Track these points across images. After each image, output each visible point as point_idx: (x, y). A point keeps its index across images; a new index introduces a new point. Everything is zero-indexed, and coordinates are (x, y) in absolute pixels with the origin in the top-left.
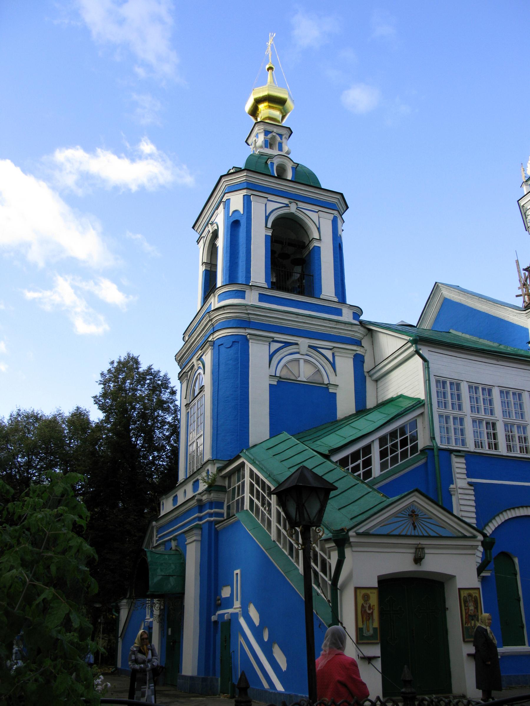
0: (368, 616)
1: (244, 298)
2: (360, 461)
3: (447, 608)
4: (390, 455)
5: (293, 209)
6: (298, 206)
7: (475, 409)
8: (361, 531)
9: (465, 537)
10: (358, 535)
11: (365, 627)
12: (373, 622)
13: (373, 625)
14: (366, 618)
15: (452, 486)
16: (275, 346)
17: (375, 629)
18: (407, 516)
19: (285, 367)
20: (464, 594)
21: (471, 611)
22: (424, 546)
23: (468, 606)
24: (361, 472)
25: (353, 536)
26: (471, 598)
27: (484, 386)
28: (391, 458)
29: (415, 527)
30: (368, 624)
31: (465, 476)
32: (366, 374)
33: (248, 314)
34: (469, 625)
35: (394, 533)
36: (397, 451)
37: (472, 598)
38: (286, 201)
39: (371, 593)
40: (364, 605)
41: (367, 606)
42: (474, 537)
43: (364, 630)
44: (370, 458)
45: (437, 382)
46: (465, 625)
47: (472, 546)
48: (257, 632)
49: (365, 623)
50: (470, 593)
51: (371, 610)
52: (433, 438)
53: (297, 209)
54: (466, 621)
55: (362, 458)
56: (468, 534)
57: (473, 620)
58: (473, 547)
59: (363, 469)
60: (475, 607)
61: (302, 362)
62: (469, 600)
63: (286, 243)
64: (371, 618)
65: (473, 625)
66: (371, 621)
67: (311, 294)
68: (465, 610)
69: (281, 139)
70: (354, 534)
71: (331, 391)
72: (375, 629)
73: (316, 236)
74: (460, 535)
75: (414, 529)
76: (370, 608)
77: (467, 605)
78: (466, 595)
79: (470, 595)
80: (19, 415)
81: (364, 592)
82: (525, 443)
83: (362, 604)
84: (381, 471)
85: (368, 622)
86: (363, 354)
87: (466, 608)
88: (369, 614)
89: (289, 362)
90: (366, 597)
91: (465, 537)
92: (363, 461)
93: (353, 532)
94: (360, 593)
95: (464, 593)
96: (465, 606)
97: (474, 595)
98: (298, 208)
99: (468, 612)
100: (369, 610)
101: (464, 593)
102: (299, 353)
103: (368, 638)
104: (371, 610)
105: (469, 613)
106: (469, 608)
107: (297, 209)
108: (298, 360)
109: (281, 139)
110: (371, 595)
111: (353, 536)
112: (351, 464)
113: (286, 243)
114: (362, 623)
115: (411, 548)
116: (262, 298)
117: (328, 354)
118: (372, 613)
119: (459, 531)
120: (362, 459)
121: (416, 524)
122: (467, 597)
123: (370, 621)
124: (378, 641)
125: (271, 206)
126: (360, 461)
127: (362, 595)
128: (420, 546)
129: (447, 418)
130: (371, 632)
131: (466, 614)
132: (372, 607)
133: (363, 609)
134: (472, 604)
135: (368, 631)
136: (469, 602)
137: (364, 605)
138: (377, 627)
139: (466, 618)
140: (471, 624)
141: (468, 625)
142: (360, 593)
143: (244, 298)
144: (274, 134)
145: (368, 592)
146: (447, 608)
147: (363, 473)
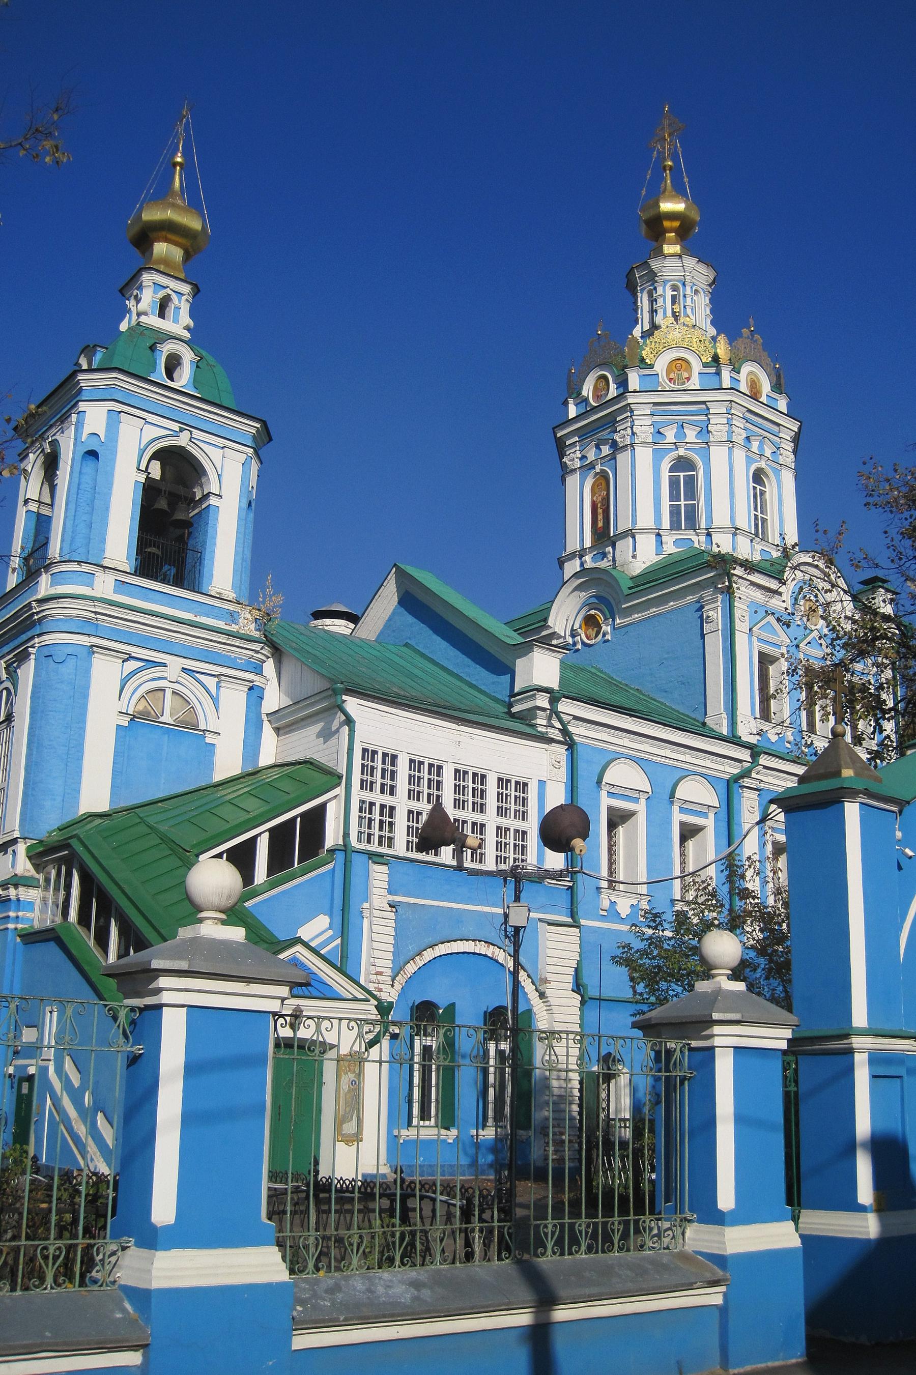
1: (91, 585)
5: (183, 440)
6: (193, 436)
7: (501, 811)
9: (355, 999)
15: (365, 905)
16: (133, 665)
19: (143, 699)
27: (432, 761)
31: (385, 892)
32: (264, 717)
33: (96, 613)
38: (176, 427)
45: (365, 751)
48: (76, 1097)
52: (346, 835)
53: (190, 441)
61: (168, 693)
63: (165, 491)
67: (194, 588)
69: (180, 301)
71: (208, 740)
73: (214, 488)
82: (523, 806)
86: (263, 686)
89: (148, 692)
91: (355, 999)
98: (193, 440)
102: (166, 679)
107: (190, 441)
108: (163, 690)
109: (180, 301)
113: (165, 491)
116: (120, 585)
117: (211, 683)
125: (151, 432)
129: (372, 804)
143: (91, 585)
144: (170, 292)
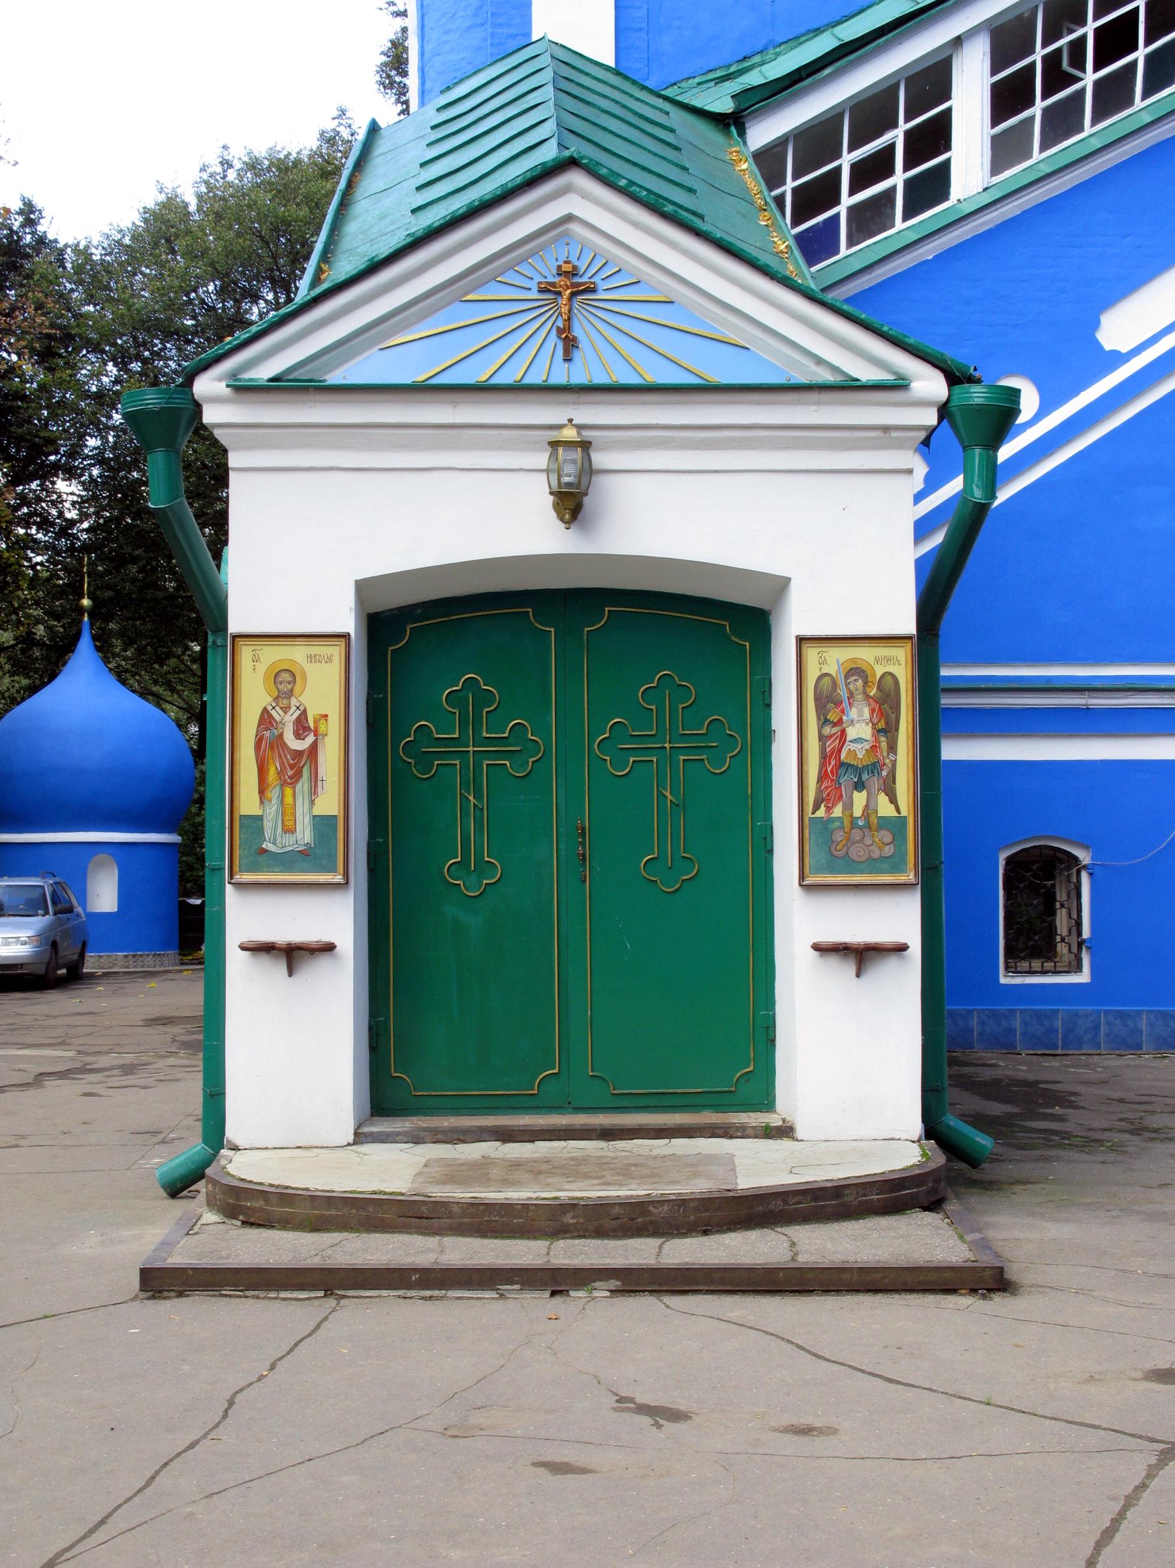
0: (292, 767)
2: (897, 136)
3: (774, 731)
4: (1044, 98)
8: (264, 373)
9: (850, 387)
10: (243, 389)
11: (271, 810)
12: (314, 791)
13: (312, 802)
14: (280, 774)
17: (323, 825)
18: (536, 295)
20: (834, 660)
21: (853, 747)
22: (588, 434)
23: (840, 721)
24: (899, 179)
25: (217, 400)
26: (860, 683)
28: (1046, 112)
29: (570, 344)
30: (289, 799)
34: (838, 811)
35: (500, 379)
36: (1082, 79)
37: (866, 683)
39: (311, 658)
40: (273, 713)
41: (290, 718)
42: (900, 385)
43: (268, 826)
44: (945, 119)
46: (816, 808)
47: (886, 429)
49: (274, 794)
50: (853, 660)
51: (310, 739)
54: (819, 791)
55: (907, 120)
56: (866, 373)
57: (859, 786)
58: (894, 434)
59: (908, 166)
60: (882, 725)
62: (851, 696)
64: (306, 771)
65: (858, 812)
66: (303, 784)
68: (822, 738)
70: (221, 388)
72: (323, 825)
74: (827, 377)
75: (568, 359)
76: (302, 727)
77: (832, 716)
78: (832, 669)
79: (856, 671)
80: (226, 164)
81: (272, 654)
83: (265, 710)
84: (996, 169)
85: (288, 791)
87: (827, 730)
88: (298, 754)
90: (285, 676)
92: (908, 134)
93: (220, 380)
94: (256, 660)
95: (823, 662)
96: (824, 721)
97: (879, 671)
99: (840, 751)
100: (298, 736)
101: (823, 662)
103: (287, 861)
104: (310, 739)
105: (843, 756)
106: (843, 732)
110: (312, 670)
111: (217, 400)
112: (850, 150)
114: (257, 797)
115: (530, 447)
118: (314, 749)
119: (819, 361)
120: (903, 126)
121: (577, 332)
122: (841, 681)
123: (299, 786)
124: (910, 877)
126: (897, 136)
127: (262, 668)
128: (570, 434)
130: (305, 835)
131: (824, 758)
132: (312, 725)
133: (267, 734)
134: (866, 712)
135: (290, 830)
136: (845, 704)
137: (271, 716)
138: (335, 813)
139: (823, 776)
140: (849, 806)
141: (829, 809)
142: (256, 660)
145: (298, 654)
146: (774, 731)
147: (908, 183)
